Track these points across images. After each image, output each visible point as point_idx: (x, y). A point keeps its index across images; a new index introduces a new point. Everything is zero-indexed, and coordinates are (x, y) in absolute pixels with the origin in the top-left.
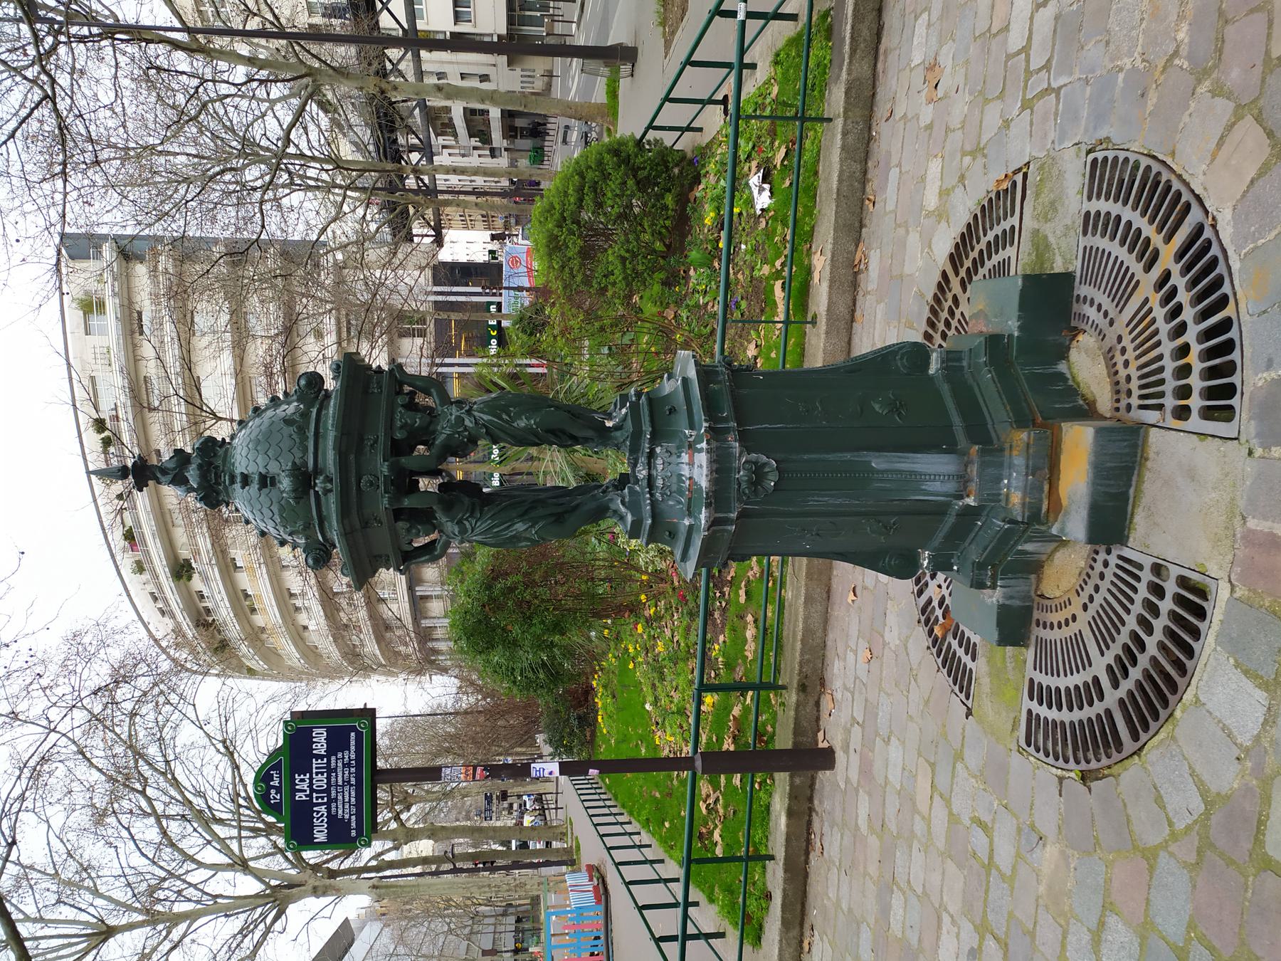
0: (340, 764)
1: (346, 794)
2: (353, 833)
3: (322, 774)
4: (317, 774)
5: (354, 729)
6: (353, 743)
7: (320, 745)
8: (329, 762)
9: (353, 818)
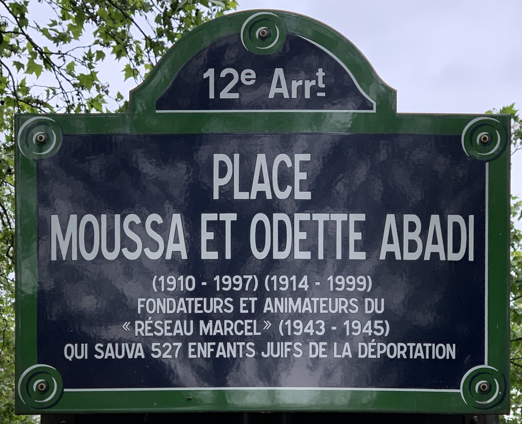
0: (340, 306)
1: (230, 328)
3: (309, 245)
4: (308, 227)
8: (346, 267)
9: (137, 352)
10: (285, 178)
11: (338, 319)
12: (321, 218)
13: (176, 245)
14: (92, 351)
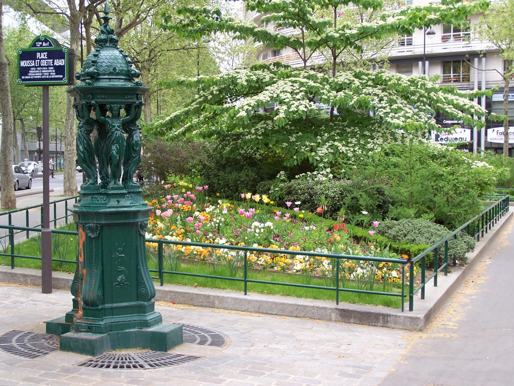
0: (50, 71)
2: (23, 77)
5: (64, 77)
6: (58, 76)
7: (59, 62)
8: (51, 66)
9: (29, 77)
10: (45, 55)
11: (49, 73)
12: (48, 60)
13: (411, 312)
14: (53, 62)
